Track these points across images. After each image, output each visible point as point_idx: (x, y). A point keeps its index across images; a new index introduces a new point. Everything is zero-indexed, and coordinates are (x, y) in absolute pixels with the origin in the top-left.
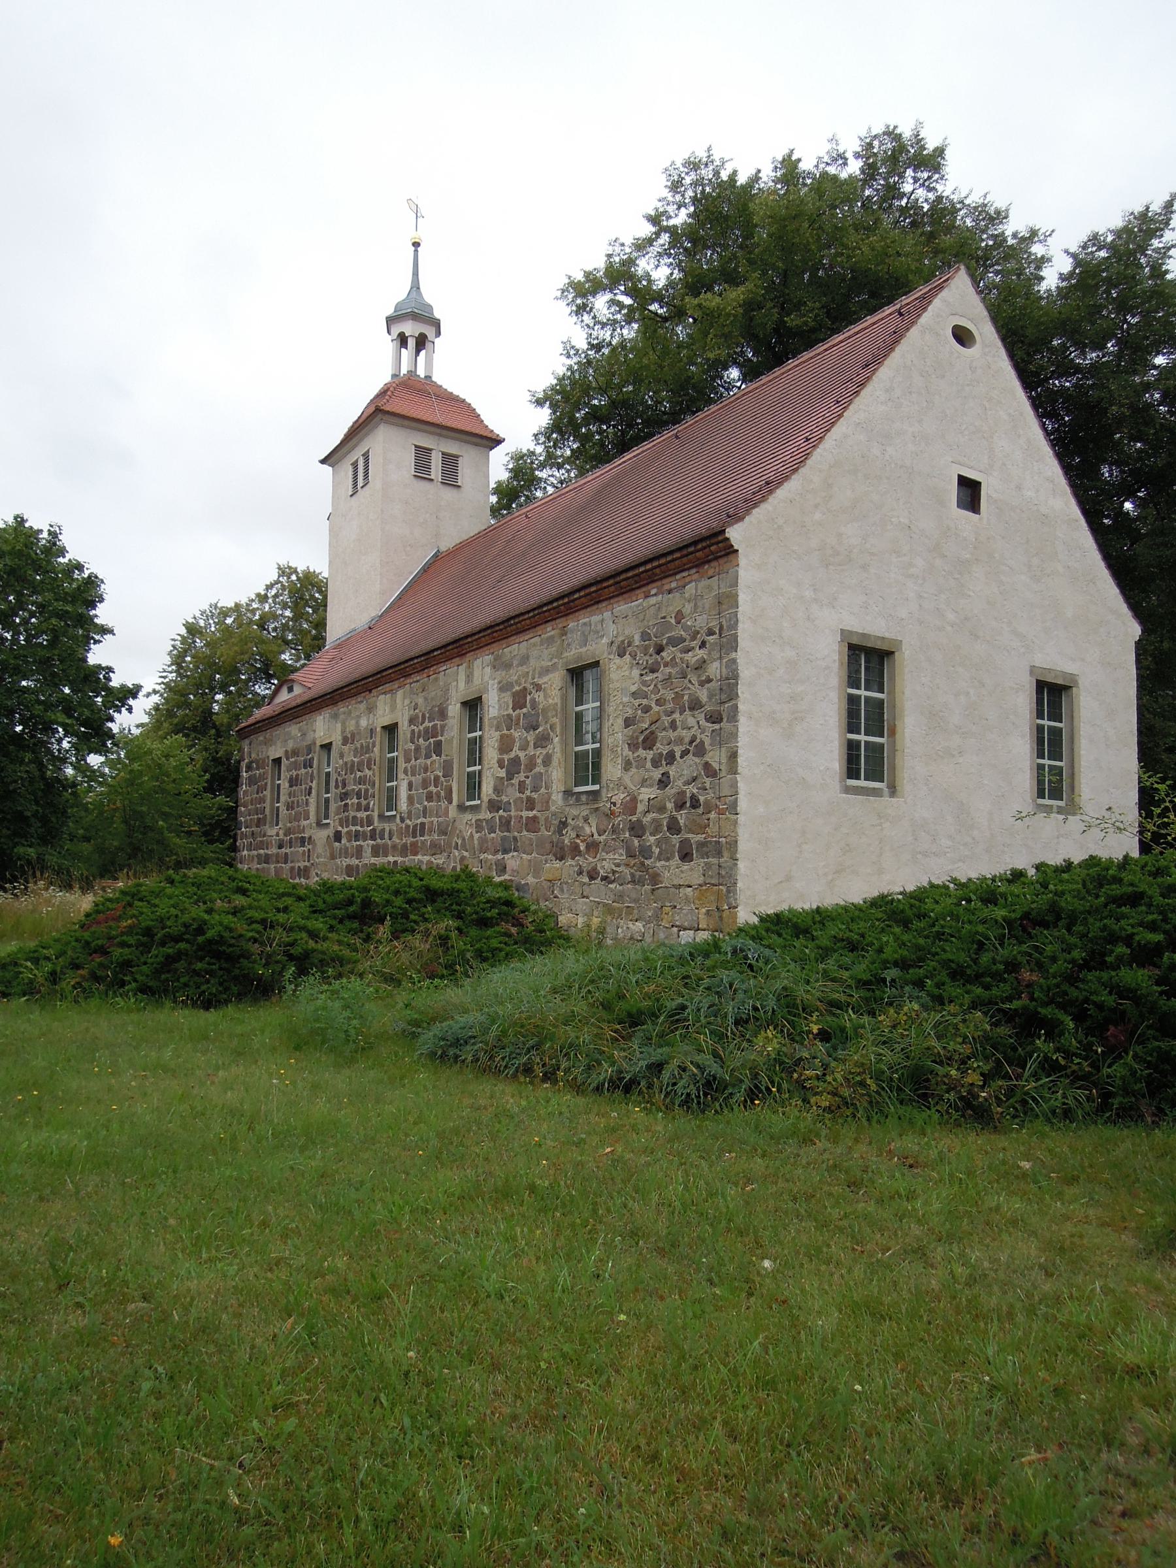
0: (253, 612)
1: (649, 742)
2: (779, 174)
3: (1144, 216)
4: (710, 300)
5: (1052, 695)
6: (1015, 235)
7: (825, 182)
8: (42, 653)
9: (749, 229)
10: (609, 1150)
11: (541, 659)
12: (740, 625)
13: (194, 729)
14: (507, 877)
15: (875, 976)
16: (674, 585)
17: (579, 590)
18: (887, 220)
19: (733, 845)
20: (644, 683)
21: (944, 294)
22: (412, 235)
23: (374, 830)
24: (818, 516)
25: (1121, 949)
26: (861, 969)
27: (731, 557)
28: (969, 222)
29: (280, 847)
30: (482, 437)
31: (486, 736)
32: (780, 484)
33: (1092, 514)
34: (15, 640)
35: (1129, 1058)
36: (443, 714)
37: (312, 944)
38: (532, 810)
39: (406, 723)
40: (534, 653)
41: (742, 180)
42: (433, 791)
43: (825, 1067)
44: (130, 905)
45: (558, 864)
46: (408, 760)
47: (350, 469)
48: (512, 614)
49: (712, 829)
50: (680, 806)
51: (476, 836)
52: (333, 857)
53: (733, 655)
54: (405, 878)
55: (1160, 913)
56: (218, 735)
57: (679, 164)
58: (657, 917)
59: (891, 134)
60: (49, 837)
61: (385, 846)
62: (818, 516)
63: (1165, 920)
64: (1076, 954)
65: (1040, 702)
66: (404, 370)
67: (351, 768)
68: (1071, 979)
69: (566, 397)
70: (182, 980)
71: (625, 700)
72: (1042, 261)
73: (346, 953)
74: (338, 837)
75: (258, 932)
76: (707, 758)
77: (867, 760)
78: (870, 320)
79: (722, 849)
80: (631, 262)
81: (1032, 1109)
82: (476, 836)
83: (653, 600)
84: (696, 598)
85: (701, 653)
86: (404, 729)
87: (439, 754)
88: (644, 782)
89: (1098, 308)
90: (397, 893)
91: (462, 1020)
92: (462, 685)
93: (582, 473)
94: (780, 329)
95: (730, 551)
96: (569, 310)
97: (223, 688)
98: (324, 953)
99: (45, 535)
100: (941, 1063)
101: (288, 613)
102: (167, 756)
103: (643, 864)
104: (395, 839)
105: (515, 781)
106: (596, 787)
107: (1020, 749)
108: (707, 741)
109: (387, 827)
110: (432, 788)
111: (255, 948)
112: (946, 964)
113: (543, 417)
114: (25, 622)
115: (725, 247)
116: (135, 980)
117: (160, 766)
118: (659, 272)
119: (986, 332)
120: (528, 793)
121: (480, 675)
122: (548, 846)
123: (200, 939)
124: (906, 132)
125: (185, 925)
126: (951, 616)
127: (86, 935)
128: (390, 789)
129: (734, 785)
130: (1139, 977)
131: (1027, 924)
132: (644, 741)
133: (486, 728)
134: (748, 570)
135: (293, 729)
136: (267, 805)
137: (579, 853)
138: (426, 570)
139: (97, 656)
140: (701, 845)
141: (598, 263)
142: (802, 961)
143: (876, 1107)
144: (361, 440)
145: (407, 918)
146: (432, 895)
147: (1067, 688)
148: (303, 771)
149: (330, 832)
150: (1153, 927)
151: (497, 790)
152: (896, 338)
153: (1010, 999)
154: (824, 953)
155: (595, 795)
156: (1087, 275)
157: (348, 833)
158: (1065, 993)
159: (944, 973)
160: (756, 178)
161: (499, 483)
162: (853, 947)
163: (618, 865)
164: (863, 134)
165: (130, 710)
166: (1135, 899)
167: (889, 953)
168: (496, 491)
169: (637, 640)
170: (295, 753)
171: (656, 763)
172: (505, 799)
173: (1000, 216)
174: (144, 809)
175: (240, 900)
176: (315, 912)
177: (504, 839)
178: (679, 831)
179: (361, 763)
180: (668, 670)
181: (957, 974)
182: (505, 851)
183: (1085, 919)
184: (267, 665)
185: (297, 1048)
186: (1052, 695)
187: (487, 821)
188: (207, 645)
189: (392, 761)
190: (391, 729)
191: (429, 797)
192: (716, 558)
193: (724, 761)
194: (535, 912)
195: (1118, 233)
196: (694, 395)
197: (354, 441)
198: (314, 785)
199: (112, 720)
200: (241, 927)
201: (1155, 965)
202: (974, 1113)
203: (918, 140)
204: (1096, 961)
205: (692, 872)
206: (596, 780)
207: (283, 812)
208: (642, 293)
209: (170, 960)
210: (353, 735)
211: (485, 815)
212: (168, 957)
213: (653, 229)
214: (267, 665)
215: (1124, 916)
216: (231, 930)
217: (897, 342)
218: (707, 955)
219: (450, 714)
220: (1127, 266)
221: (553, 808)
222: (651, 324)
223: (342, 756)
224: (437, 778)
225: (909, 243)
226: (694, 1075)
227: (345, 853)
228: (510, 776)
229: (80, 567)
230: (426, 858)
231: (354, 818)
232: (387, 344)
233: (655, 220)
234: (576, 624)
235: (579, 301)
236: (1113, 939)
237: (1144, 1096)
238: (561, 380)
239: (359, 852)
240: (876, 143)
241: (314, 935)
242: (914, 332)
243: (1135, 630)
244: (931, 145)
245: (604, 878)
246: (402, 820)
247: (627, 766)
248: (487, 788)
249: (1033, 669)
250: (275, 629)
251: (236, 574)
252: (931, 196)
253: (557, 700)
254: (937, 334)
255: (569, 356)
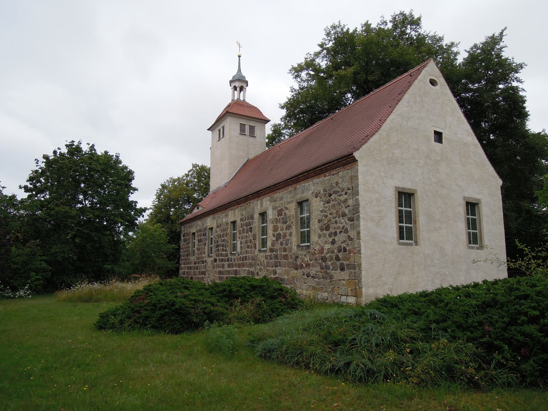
0: (184, 180)
1: (327, 228)
2: (363, 29)
3: (493, 37)
4: (342, 72)
5: (472, 207)
6: (446, 46)
7: (380, 32)
8: (113, 197)
9: (353, 48)
10: (336, 404)
11: (287, 198)
12: (359, 186)
13: (164, 221)
14: (277, 276)
15: (427, 327)
16: (335, 172)
17: (301, 174)
18: (402, 43)
19: (360, 265)
20: (325, 207)
21: (426, 68)
22: (238, 53)
23: (228, 258)
24: (385, 147)
25: (524, 318)
26: (421, 323)
27: (355, 163)
28: (430, 42)
29: (195, 264)
30: (262, 120)
31: (268, 226)
32: (372, 136)
33: (480, 140)
34: (104, 193)
35: (531, 362)
36: (252, 217)
37: (212, 308)
38: (285, 252)
39: (239, 221)
40: (285, 196)
41: (351, 31)
42: (250, 244)
43: (413, 365)
44: (147, 293)
45: (295, 271)
46: (240, 234)
47: (218, 132)
48: (277, 182)
49: (352, 259)
50: (340, 251)
51: (265, 261)
52: (214, 268)
53: (357, 197)
54: (244, 281)
55: (537, 303)
56: (172, 223)
57: (329, 27)
58: (332, 291)
59: (402, 14)
60: (115, 261)
61: (232, 264)
62: (385, 147)
63: (539, 305)
64: (505, 319)
65: (467, 209)
66: (236, 98)
67: (220, 236)
68: (505, 329)
69: (292, 106)
70: (167, 323)
71: (318, 213)
72: (456, 54)
73: (225, 311)
74: (215, 260)
75: (193, 304)
76: (349, 234)
77: (407, 233)
78: (399, 78)
79: (356, 267)
80: (313, 60)
81: (495, 382)
82: (265, 261)
83: (327, 178)
84: (343, 177)
85: (345, 196)
86: (239, 223)
87: (251, 232)
88: (326, 242)
89: (478, 69)
90: (241, 287)
91: (271, 341)
92: (259, 207)
93: (297, 131)
94: (366, 82)
95: (355, 161)
96: (292, 77)
97: (174, 206)
98: (216, 311)
99: (114, 157)
100: (457, 363)
101: (196, 180)
102: (155, 231)
103: (326, 272)
104: (236, 262)
105: (279, 242)
106: (309, 244)
107: (461, 227)
108: (349, 228)
109: (233, 257)
110: (249, 244)
111: (192, 311)
112: (455, 322)
113: (284, 112)
114: (108, 187)
115: (345, 54)
116: (150, 323)
117: (153, 235)
118: (323, 63)
119: (441, 80)
120: (284, 246)
121: (265, 204)
122: (292, 265)
123: (173, 308)
124: (407, 13)
125: (167, 302)
126: (434, 180)
127: (133, 306)
128: (234, 244)
129: (359, 243)
130: (532, 329)
131: (484, 306)
132: (326, 228)
133: (268, 223)
134: (361, 167)
135: (199, 222)
136: (190, 249)
137: (303, 267)
138: (244, 165)
139: (132, 198)
140: (348, 265)
141: (302, 61)
142: (397, 319)
143: (435, 384)
144: (221, 122)
145: (245, 296)
146: (254, 287)
147: (477, 204)
148: (203, 237)
149: (213, 259)
150: (534, 308)
151: (272, 245)
152: (410, 84)
153: (482, 337)
154: (405, 316)
155: (308, 247)
156: (472, 59)
157: (219, 259)
158: (503, 335)
159: (454, 326)
160: (355, 30)
161: (269, 135)
162: (416, 313)
163: (317, 272)
164: (393, 14)
165: (143, 216)
166: (526, 297)
167: (431, 317)
168: (268, 138)
169: (322, 192)
170: (200, 231)
171: (330, 236)
172: (276, 248)
173: (441, 39)
174: (147, 250)
175: (187, 292)
176: (212, 294)
177: (275, 262)
178: (339, 260)
179: (223, 235)
180: (334, 202)
181: (459, 327)
182: (276, 267)
183: (507, 305)
184: (189, 198)
185: (210, 352)
186: (472, 207)
187: (269, 256)
188: (168, 192)
189: (234, 234)
190: (234, 223)
191: (248, 247)
192: (350, 163)
193: (355, 235)
194: (290, 293)
195: (484, 44)
196: (336, 104)
197: (219, 123)
198: (207, 242)
199: (137, 220)
200: (187, 303)
201: (537, 324)
202: (473, 385)
203: (411, 15)
204: (513, 322)
205: (345, 275)
206: (309, 241)
207: (196, 251)
208: (317, 70)
209: (163, 315)
210: (220, 225)
211: (268, 253)
212: (162, 314)
213: (321, 49)
214: (189, 198)
215: (523, 304)
216: (184, 304)
217: (410, 86)
218: (360, 316)
219: (255, 217)
220: (488, 55)
221: (293, 251)
222: (321, 81)
223: (216, 232)
224: (251, 240)
225: (411, 50)
226: (363, 368)
227: (218, 266)
228: (277, 240)
229: (126, 168)
230: (248, 268)
231: (221, 254)
232: (230, 89)
233: (321, 46)
234: (300, 186)
235: (296, 74)
236: (519, 313)
237: (539, 377)
238: (290, 100)
239: (223, 266)
240: (397, 17)
241: (212, 304)
242: (416, 82)
243: (500, 182)
244: (416, 17)
245: (312, 277)
246: (238, 255)
247: (320, 236)
248: (269, 244)
249: (464, 198)
250: (191, 186)
251: (180, 168)
252: (416, 33)
253: (294, 213)
254: (424, 82)
255: (292, 92)
